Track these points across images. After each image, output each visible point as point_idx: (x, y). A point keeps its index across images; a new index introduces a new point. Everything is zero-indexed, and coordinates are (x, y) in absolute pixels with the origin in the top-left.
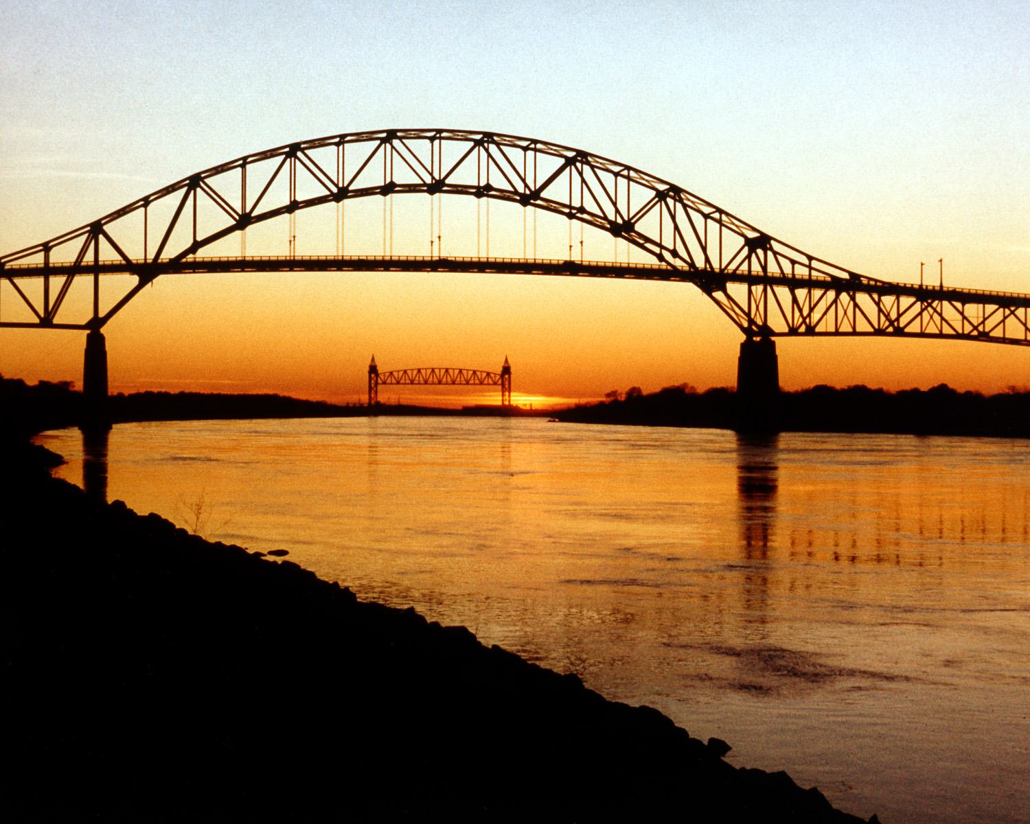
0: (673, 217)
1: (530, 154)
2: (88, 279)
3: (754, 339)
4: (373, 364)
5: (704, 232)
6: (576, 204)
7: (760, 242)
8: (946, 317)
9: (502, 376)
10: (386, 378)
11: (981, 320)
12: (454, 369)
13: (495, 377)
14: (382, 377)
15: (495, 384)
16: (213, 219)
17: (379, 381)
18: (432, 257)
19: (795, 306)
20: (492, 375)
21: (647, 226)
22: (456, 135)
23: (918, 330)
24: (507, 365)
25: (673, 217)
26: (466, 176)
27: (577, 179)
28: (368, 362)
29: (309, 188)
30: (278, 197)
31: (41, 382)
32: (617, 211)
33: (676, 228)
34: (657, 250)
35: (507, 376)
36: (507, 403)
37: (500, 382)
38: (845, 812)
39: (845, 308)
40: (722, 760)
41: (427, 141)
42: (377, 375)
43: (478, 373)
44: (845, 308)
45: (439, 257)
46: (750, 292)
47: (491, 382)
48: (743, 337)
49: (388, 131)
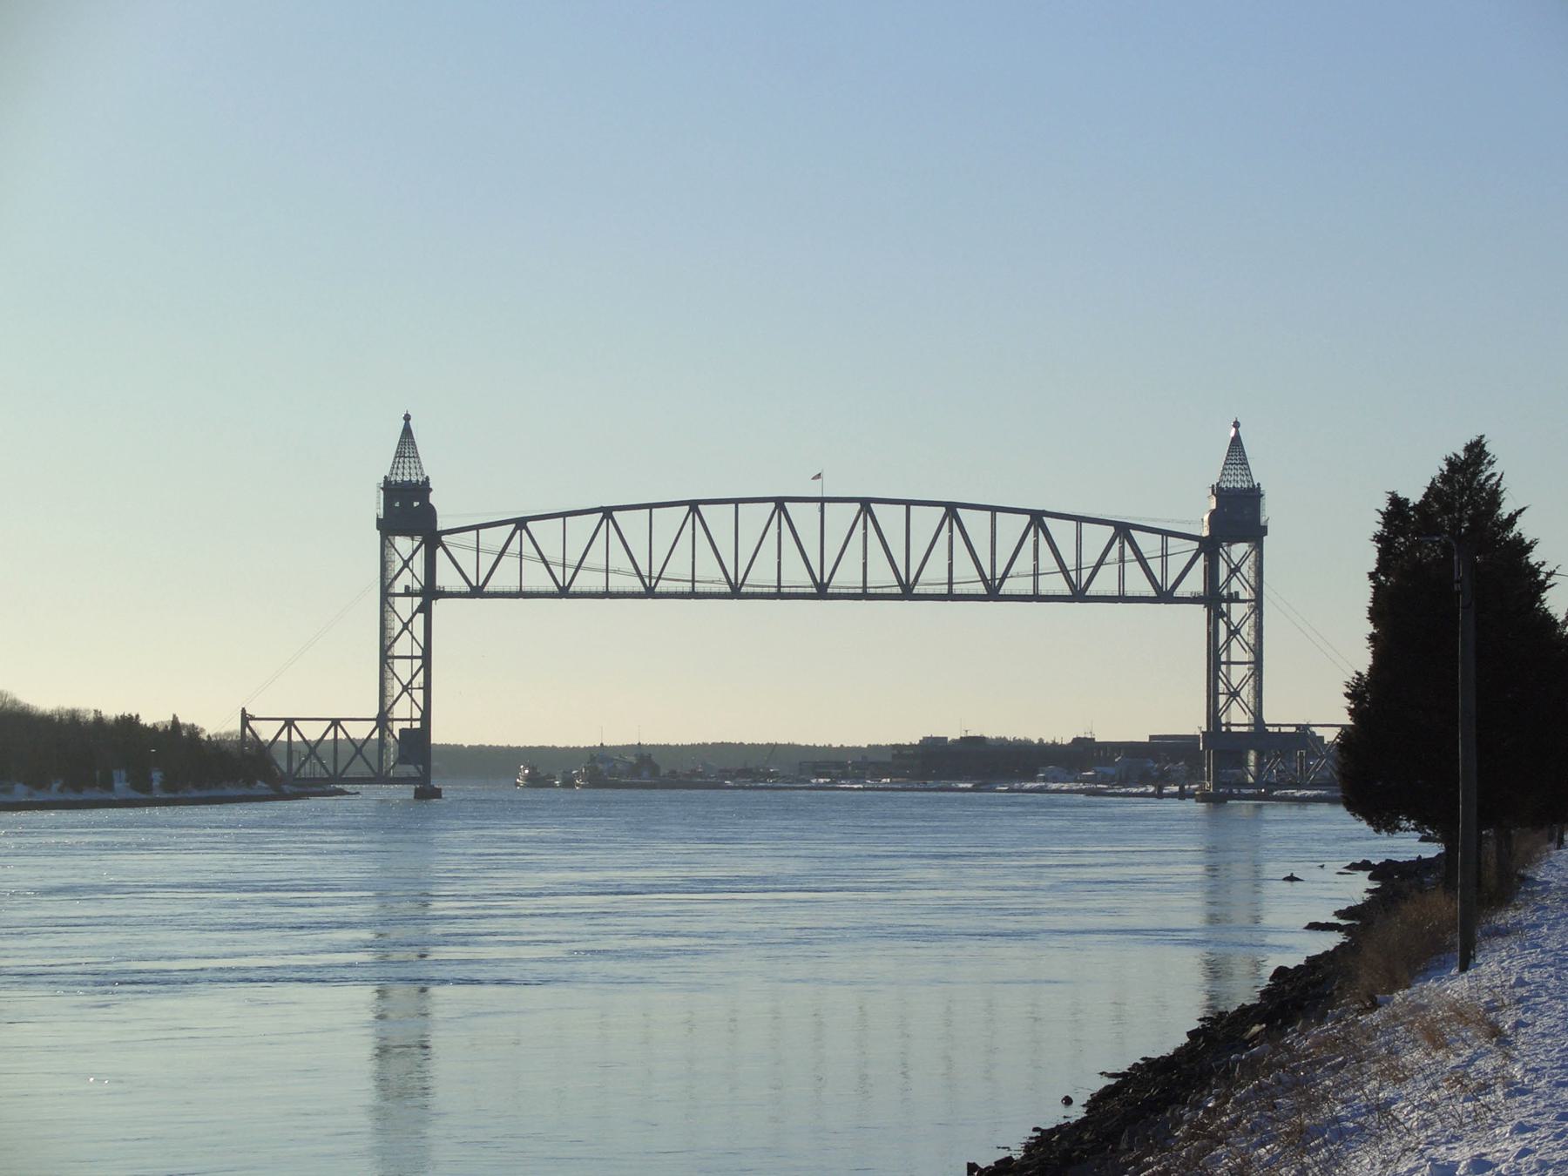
4: (407, 475)
9: (1209, 548)
10: (487, 562)
14: (467, 560)
15: (1164, 596)
17: (447, 578)
19: (954, 523)
20: (1149, 544)
23: (1113, 590)
24: (1240, 483)
28: (380, 464)
31: (924, 738)
35: (1239, 550)
36: (1238, 717)
37: (1195, 583)
38: (1077, 1113)
42: (432, 540)
45: (413, 540)
47: (1137, 583)
49: (389, 527)
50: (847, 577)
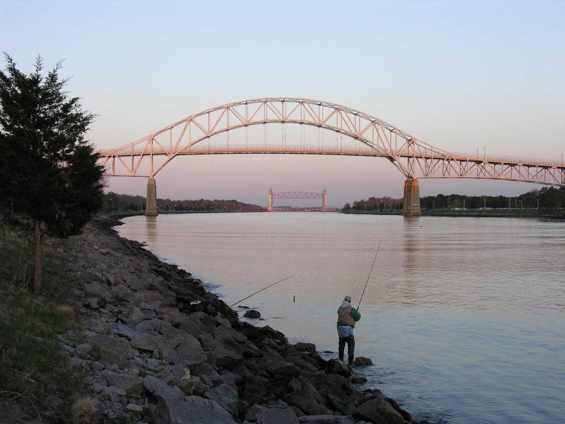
0: (377, 131)
1: (321, 106)
2: (149, 157)
3: (72, 165)
5: (224, 113)
6: (339, 127)
7: (410, 141)
8: (522, 174)
11: (501, 171)
12: (298, 192)
13: (320, 195)
16: (197, 134)
18: (282, 148)
21: (367, 136)
22: (329, 105)
25: (377, 131)
26: (296, 116)
27: (339, 116)
28: (323, 190)
29: (234, 121)
30: (222, 125)
32: (355, 130)
33: (379, 135)
34: (372, 145)
39: (464, 168)
40: (345, 343)
41: (281, 102)
43: (313, 194)
44: (464, 168)
46: (409, 160)
48: (406, 179)
50: (300, 197)
